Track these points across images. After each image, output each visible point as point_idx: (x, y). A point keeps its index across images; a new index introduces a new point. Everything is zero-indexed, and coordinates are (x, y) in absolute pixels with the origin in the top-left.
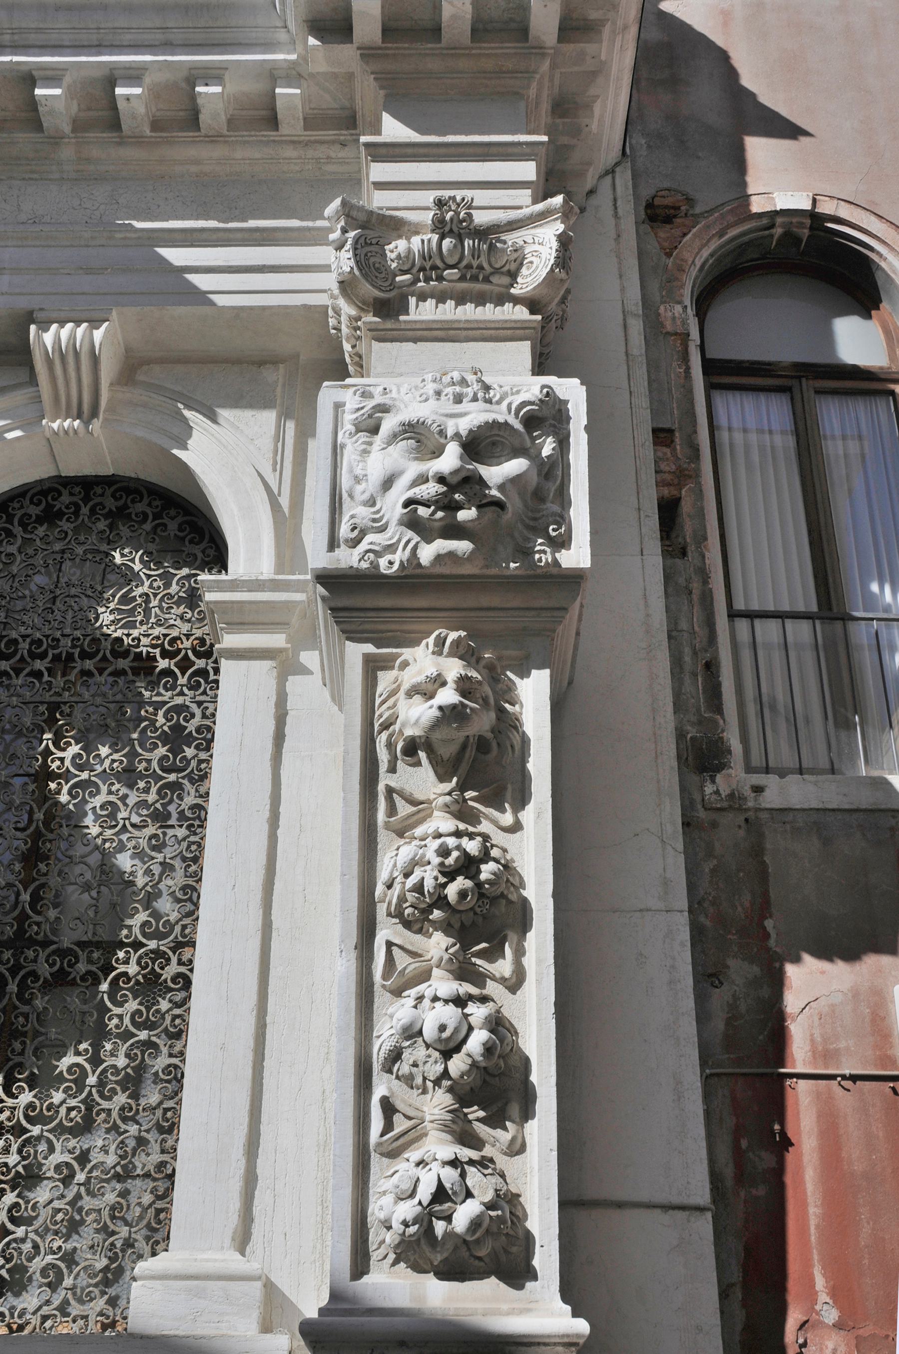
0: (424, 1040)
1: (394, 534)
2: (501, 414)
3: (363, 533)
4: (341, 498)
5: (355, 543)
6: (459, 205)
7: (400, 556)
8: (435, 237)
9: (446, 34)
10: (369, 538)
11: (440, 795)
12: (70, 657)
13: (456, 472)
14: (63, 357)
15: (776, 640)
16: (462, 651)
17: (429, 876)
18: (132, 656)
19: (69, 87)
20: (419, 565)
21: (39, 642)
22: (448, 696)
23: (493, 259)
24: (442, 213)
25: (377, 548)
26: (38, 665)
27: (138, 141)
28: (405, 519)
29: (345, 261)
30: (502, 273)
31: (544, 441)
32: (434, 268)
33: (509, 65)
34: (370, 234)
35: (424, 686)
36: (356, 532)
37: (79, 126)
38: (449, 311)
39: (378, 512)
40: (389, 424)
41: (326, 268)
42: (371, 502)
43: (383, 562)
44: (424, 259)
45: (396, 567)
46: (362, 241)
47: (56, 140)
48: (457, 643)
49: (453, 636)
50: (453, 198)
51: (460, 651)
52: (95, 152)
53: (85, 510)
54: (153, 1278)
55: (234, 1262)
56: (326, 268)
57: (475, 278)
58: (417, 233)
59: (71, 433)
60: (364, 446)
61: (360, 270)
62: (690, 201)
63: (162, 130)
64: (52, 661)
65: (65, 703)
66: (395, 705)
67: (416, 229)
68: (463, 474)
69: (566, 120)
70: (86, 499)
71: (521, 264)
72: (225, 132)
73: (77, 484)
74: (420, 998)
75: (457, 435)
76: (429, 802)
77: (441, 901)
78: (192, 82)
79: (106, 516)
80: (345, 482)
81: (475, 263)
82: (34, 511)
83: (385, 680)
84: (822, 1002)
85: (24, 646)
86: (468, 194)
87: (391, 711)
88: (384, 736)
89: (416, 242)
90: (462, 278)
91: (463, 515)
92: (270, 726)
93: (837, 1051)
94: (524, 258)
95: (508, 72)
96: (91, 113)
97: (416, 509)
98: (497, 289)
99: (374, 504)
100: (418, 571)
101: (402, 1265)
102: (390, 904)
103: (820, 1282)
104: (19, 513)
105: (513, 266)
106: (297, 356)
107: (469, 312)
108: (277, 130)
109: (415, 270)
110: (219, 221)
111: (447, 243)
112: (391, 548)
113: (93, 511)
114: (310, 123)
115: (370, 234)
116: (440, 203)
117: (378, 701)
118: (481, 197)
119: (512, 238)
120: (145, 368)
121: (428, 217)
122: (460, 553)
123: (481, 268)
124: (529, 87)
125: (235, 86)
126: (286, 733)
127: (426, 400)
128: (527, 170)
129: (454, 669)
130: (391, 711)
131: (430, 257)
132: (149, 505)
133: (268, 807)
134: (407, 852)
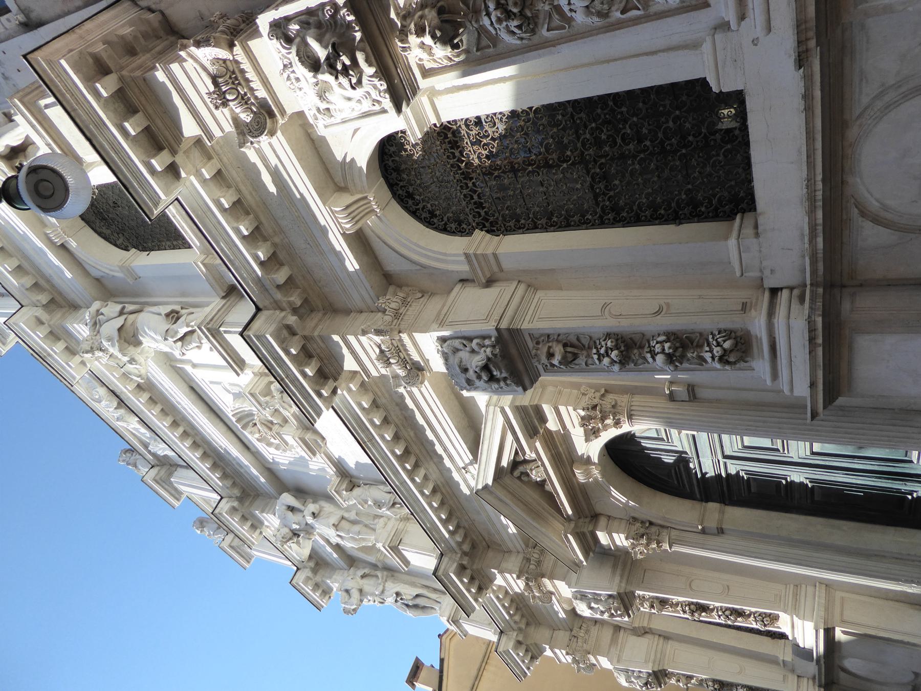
0: (590, 4)
1: (368, 87)
2: (293, 57)
3: (374, 100)
4: (363, 113)
5: (378, 102)
6: (212, 99)
7: (376, 81)
8: (231, 104)
9: (145, 124)
10: (374, 97)
11: (473, 26)
12: (450, 142)
13: (331, 74)
14: (353, 219)
16: (404, 37)
17: (513, 24)
18: (453, 151)
19: (256, 249)
20: (376, 72)
21: (461, 187)
22: (427, 40)
23: (224, 73)
24: (220, 105)
25: (378, 93)
26: (470, 185)
27: (257, 218)
28: (360, 86)
29: (264, 139)
30: (226, 66)
31: (293, 29)
32: (242, 98)
33: (136, 90)
34: (246, 131)
35: (428, 51)
36: (375, 103)
37: (265, 239)
38: (256, 84)
39: (362, 97)
40: (323, 106)
41: (270, 144)
42: (359, 101)
43: (382, 88)
44: (228, 83)
45: (382, 82)
46: (251, 134)
47: (275, 245)
48: (402, 41)
49: (399, 44)
50: (211, 102)
51: (404, 40)
52: (270, 231)
53: (401, 184)
54: (719, 83)
55: (707, 47)
56: (270, 144)
57: (236, 78)
58: (233, 111)
59: (378, 204)
60: (337, 111)
61: (264, 132)
63: (248, 211)
64: (453, 149)
65: (482, 171)
66: (440, 58)
67: (232, 110)
68: (330, 70)
69: (135, 46)
70: (398, 185)
71: (218, 59)
72: (234, 188)
73: (393, 190)
74: (571, 10)
75: (314, 77)
76: (477, 29)
77: (522, 14)
78: (225, 210)
79: (400, 175)
80: (356, 114)
81: (230, 81)
82: (410, 202)
83: (428, 65)
85: (465, 191)
86: (206, 97)
87: (444, 60)
88: (455, 59)
89: (238, 110)
90: (239, 84)
91: (348, 62)
92: (463, 93)
94: (214, 58)
95: (139, 89)
96: (258, 237)
97: (354, 84)
98: (235, 66)
99: (359, 100)
100: (378, 71)
102: (530, 36)
104: (414, 207)
105: (221, 62)
106: (300, 125)
107: (251, 75)
108: (220, 169)
109: (249, 106)
111: (229, 97)
112: (375, 87)
113: (400, 181)
114: (210, 158)
115: (246, 131)
116: (217, 108)
117: (441, 66)
118: (204, 91)
119: (211, 69)
120: (338, 184)
121: (226, 111)
122: (364, 56)
123: (230, 78)
124: (138, 77)
125: (217, 193)
126: (462, 84)
127: (305, 93)
128: (175, 67)
129: (413, 40)
130: (444, 60)
131: (240, 102)
132: (388, 160)
133: (499, 84)
134: (504, 35)
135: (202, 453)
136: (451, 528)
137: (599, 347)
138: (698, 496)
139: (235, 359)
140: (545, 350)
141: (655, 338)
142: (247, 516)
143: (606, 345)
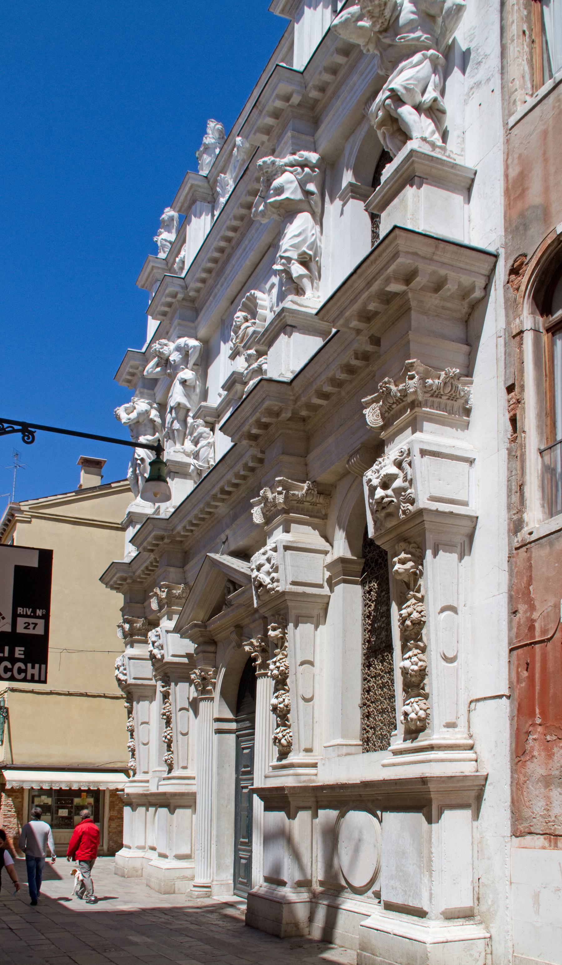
15: (547, 550)
62: (525, 256)
84: (545, 612)
93: (548, 629)
101: (441, 553)
103: (537, 711)
110: (370, 395)
137: (281, 661)
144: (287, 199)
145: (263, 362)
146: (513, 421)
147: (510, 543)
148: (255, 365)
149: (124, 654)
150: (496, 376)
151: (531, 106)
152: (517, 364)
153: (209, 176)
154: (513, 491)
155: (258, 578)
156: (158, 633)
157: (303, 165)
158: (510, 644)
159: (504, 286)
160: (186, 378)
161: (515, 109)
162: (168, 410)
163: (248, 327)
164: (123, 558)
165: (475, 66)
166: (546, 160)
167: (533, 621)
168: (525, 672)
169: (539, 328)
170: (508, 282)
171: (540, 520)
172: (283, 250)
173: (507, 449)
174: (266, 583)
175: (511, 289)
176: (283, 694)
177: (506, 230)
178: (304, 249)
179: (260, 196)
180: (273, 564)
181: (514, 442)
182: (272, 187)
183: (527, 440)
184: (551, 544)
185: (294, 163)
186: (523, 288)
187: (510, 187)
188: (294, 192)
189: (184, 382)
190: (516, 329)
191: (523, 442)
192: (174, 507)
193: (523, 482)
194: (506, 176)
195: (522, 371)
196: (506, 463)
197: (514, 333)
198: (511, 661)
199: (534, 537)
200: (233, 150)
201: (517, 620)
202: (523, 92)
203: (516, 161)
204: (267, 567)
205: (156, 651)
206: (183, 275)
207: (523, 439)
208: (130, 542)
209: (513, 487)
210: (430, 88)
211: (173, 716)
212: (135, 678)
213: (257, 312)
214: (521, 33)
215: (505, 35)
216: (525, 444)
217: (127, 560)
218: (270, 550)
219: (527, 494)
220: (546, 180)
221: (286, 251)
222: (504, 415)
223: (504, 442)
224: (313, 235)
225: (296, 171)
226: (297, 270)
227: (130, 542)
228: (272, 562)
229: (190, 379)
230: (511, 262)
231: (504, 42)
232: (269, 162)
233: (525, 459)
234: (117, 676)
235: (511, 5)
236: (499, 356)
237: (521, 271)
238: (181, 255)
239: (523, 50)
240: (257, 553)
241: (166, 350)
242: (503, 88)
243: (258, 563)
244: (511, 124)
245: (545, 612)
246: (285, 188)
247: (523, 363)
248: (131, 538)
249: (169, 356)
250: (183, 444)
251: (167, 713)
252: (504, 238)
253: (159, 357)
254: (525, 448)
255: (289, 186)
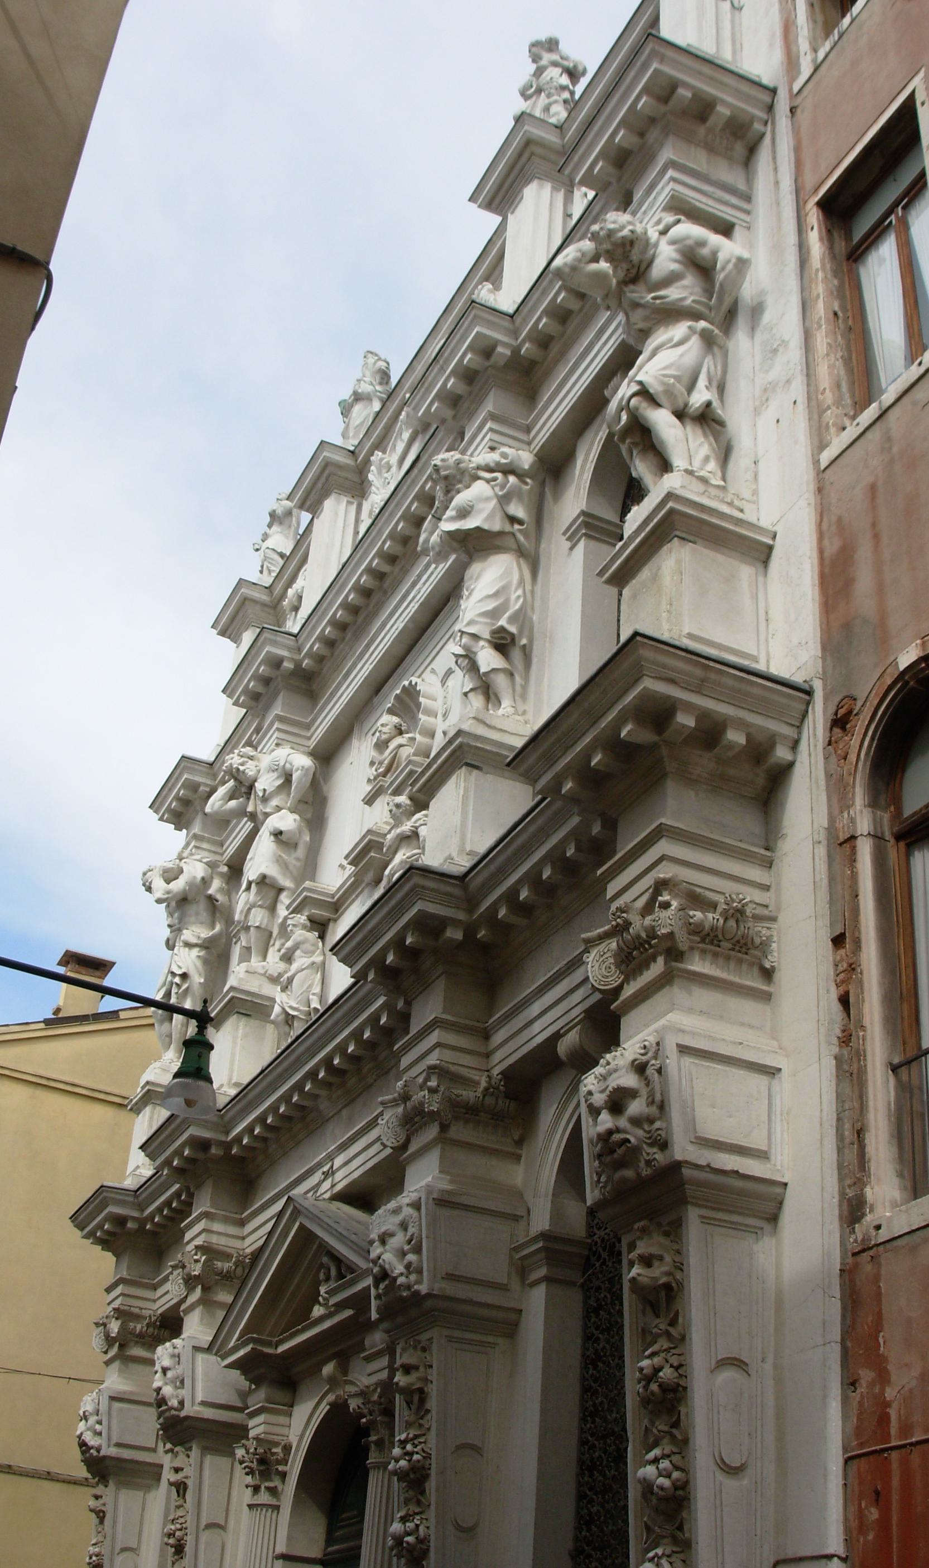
84: (906, 1389)
135: (358, 604)
136: (546, 873)
137: (416, 1442)
138: (330, 1549)
139: (433, 780)
140: (655, 1250)
141: (424, 1521)
142: (272, 685)
143: (417, 1453)
144: (478, 528)
145: (421, 822)
146: (844, 1001)
147: (843, 1244)
148: (406, 827)
149: (102, 1387)
150: (814, 915)
151: (851, 440)
152: (847, 898)
153: (357, 451)
154: (847, 1141)
155: (381, 1261)
156: (176, 1351)
157: (508, 470)
158: (845, 1450)
159: (824, 748)
160: (282, 829)
161: (829, 438)
162: (244, 886)
163: (401, 746)
164: (124, 1177)
165: (770, 355)
166: (876, 537)
167: (887, 1404)
168: (873, 1510)
169: (882, 833)
170: (829, 744)
171: (896, 1202)
172: (465, 622)
173: (836, 1058)
174: (397, 1272)
175: (834, 755)
176: (417, 1514)
177: (824, 648)
178: (503, 622)
179: (433, 516)
180: (412, 1235)
181: (847, 1046)
182: (453, 504)
183: (868, 1043)
184: (913, 1249)
185: (492, 465)
186: (852, 757)
187: (827, 570)
188: (490, 517)
189: (278, 834)
190: (844, 832)
191: (861, 1047)
192: (236, 1084)
193: (863, 1125)
194: (821, 551)
195: (855, 911)
196: (834, 1082)
197: (842, 839)
198: (848, 1485)
199: (884, 1235)
200: (400, 413)
201: (858, 1399)
202: (839, 411)
203: (834, 528)
204: (398, 1240)
205: (167, 1390)
206: (295, 631)
207: (861, 1042)
208: (141, 1148)
209: (847, 1133)
210: (702, 382)
211: (190, 1539)
212: (118, 1445)
213: (421, 703)
214: (831, 315)
215: (808, 314)
216: (864, 1051)
217: (130, 1183)
218: (408, 1205)
219: (871, 1149)
220: (878, 569)
221: (470, 623)
222: (828, 991)
223: (830, 1044)
224: (519, 597)
225: (495, 479)
226: (488, 659)
227: (141, 1148)
228: (411, 1230)
229: (289, 831)
230: (832, 709)
231: (807, 324)
232: (451, 461)
233: (866, 1080)
234: (80, 1437)
235: (814, 271)
236: (817, 879)
237: (848, 726)
238: (297, 586)
239: (836, 342)
240: (383, 1208)
241: (250, 769)
242: (809, 399)
243: (383, 1229)
244: (824, 463)
245: (906, 1389)
246: (475, 508)
247: (857, 896)
248: (144, 1139)
249: (255, 781)
250: (264, 957)
251: (178, 1533)
252: (820, 661)
253: (236, 779)
254: (865, 1060)
255: (481, 505)
